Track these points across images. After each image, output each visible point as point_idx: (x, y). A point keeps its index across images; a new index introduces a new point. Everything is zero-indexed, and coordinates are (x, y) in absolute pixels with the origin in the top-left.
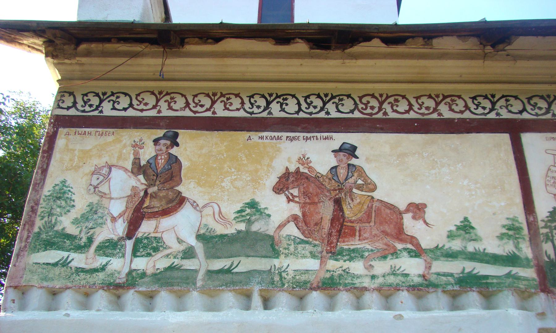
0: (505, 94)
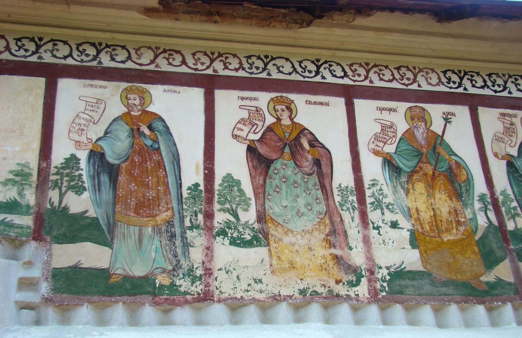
0: (54, 39)
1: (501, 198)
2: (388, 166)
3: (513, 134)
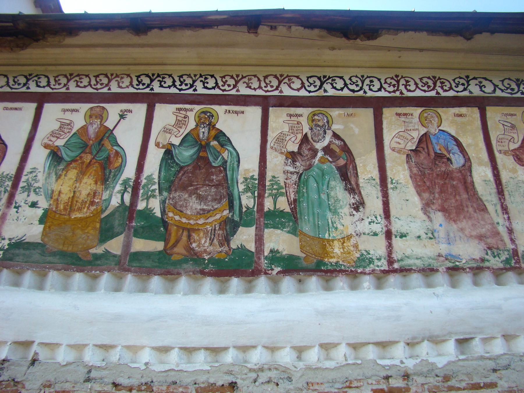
1: (144, 181)
2: (52, 158)
3: (183, 126)
